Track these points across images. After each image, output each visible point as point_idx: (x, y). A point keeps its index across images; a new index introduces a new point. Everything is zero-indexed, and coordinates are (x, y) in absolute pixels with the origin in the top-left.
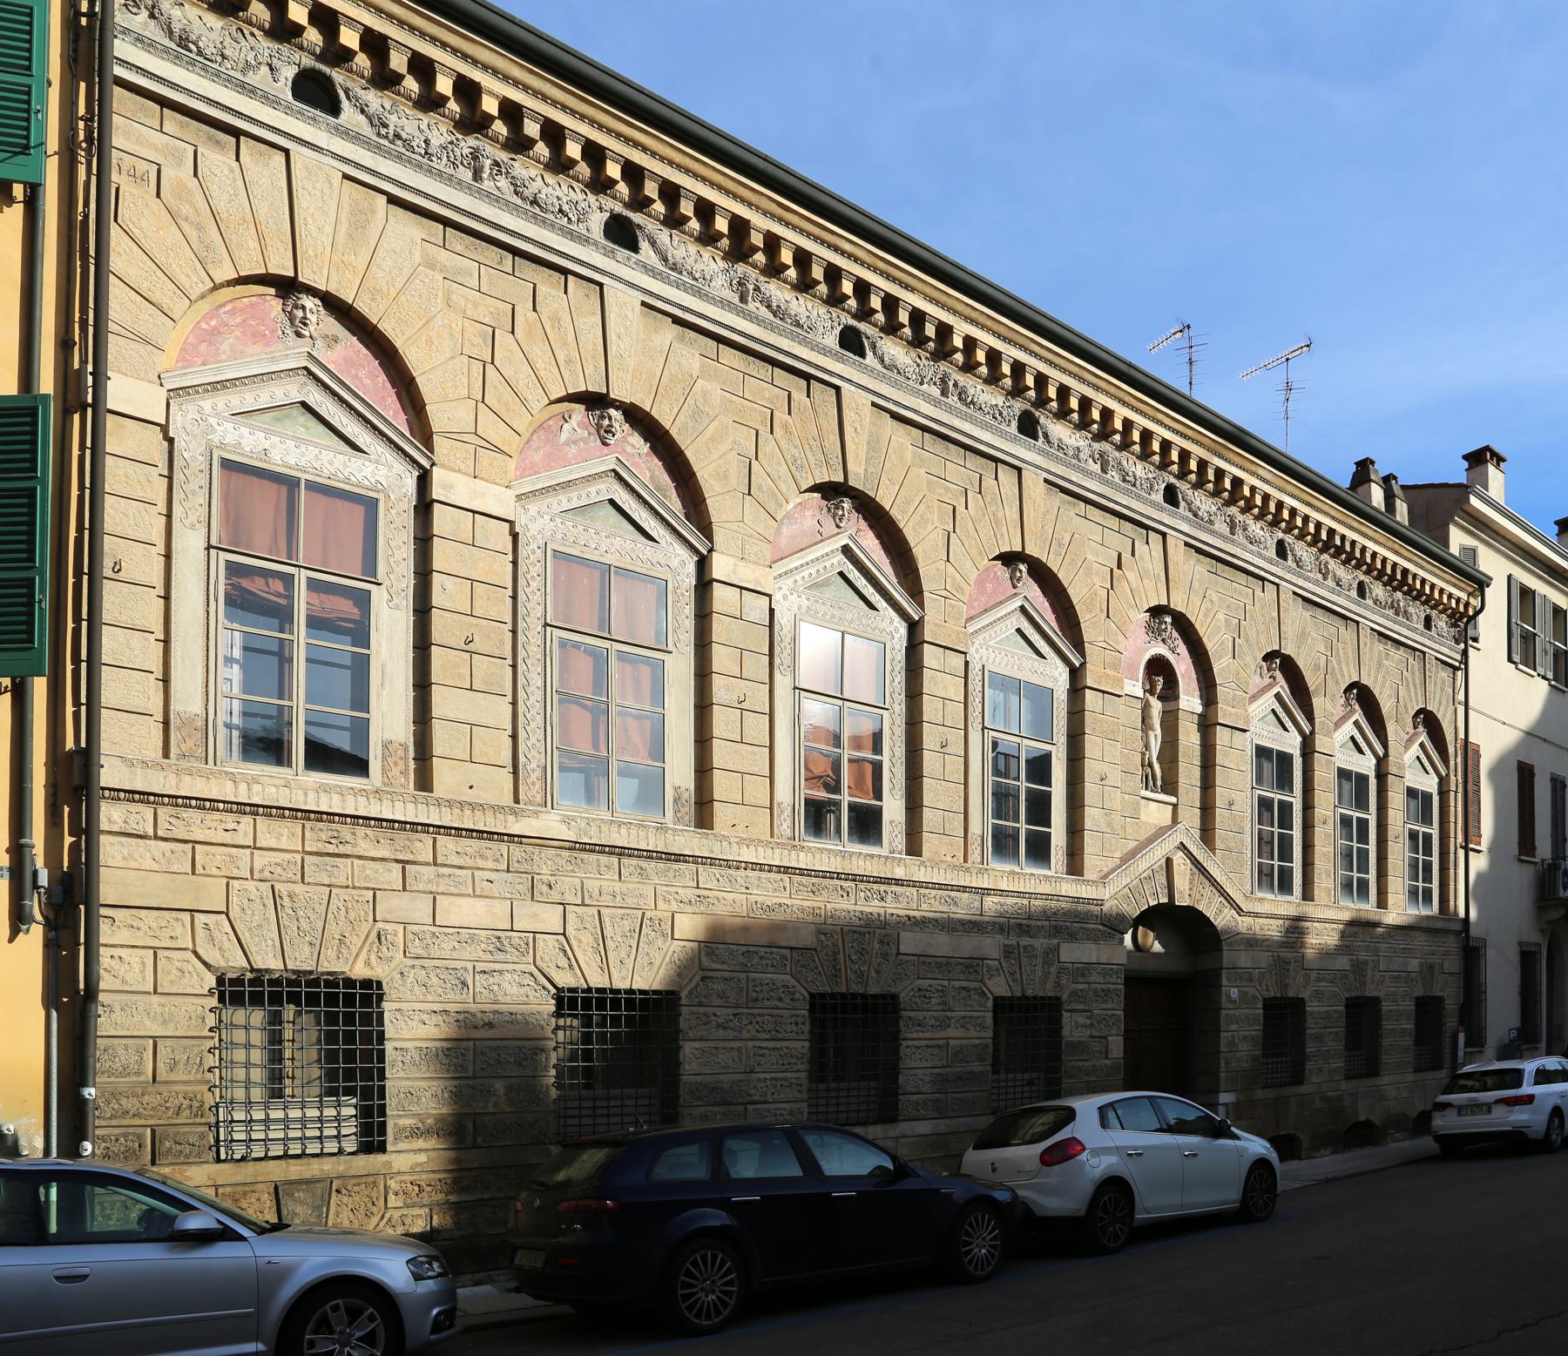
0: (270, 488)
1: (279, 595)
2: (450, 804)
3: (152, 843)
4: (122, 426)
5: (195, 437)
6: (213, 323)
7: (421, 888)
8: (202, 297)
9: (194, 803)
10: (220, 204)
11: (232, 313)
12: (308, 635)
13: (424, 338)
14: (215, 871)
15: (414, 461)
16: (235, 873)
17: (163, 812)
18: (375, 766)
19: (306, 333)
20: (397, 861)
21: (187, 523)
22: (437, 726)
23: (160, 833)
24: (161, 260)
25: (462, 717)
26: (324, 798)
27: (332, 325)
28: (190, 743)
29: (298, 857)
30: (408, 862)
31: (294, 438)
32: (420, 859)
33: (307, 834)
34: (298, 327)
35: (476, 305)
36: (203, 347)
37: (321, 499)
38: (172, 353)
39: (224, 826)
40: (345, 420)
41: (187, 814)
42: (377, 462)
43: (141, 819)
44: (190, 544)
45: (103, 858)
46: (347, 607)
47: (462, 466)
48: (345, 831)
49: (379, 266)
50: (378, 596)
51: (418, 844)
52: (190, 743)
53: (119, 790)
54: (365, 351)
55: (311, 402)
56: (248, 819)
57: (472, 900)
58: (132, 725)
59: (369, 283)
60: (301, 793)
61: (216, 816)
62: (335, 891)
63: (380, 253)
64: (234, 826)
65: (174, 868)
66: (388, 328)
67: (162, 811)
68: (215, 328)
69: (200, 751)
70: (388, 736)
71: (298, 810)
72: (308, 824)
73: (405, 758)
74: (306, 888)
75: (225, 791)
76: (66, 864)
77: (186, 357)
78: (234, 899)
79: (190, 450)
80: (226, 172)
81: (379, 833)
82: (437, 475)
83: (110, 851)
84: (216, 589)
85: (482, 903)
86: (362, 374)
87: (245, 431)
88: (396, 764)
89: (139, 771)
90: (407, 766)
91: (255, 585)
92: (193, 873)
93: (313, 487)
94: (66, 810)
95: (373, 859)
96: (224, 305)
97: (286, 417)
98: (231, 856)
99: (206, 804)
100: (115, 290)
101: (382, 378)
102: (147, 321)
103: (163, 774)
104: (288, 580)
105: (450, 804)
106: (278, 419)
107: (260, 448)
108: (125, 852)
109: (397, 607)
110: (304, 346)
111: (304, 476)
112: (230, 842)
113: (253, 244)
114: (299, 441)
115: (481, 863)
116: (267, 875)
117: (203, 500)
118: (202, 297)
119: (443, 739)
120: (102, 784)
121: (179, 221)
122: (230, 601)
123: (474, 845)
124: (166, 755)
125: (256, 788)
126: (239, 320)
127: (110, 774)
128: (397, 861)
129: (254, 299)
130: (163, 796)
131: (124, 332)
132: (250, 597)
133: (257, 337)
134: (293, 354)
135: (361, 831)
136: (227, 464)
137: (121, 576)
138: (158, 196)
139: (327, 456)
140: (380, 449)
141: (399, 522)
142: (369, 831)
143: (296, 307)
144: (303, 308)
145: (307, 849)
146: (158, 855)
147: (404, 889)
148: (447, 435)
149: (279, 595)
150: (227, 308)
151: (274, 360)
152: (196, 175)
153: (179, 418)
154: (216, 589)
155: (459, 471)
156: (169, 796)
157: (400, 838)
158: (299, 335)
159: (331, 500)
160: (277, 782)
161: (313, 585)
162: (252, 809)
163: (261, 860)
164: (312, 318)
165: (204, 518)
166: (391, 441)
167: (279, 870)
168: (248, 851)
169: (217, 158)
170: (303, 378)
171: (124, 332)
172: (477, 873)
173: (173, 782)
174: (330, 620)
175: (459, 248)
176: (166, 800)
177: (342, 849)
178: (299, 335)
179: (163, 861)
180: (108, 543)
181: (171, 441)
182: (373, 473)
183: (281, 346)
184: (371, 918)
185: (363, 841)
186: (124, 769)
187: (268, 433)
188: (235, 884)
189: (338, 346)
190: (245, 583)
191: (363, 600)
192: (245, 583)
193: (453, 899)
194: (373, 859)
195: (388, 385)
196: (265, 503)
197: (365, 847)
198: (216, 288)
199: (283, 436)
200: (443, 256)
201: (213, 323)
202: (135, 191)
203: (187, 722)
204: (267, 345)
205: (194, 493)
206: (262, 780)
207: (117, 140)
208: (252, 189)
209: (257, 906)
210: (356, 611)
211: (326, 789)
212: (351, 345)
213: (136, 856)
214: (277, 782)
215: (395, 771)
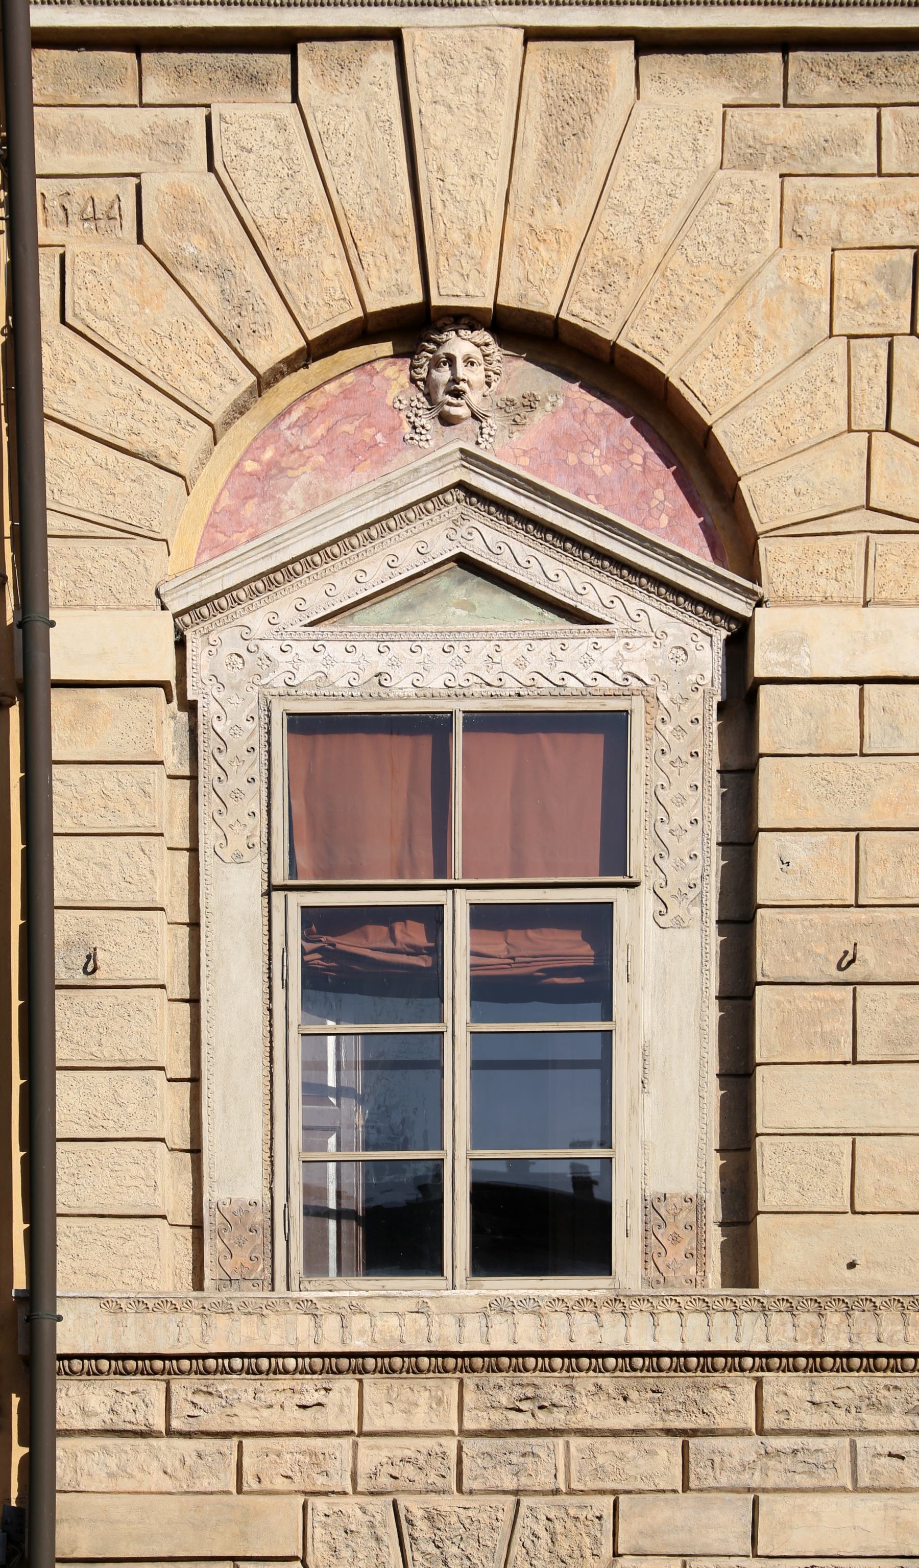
0: (402, 745)
1: (416, 951)
2: (791, 1305)
3: (162, 1443)
4: (93, 706)
5: (236, 688)
6: (268, 454)
7: (724, 1481)
8: (240, 409)
9: (237, 1363)
10: (261, 207)
11: (304, 424)
12: (476, 1017)
13: (733, 329)
14: (280, 1484)
15: (714, 609)
16: (320, 1483)
17: (182, 1387)
18: (625, 1246)
19: (462, 411)
20: (669, 1432)
21: (226, 853)
22: (765, 1148)
23: (176, 1424)
24: (149, 363)
25: (831, 1123)
26: (500, 1323)
27: (524, 375)
28: (242, 1256)
29: (451, 1445)
30: (695, 1433)
31: (438, 635)
32: (722, 1423)
33: (469, 1398)
34: (441, 403)
35: (867, 209)
36: (250, 509)
37: (506, 744)
38: (187, 537)
39: (298, 1399)
40: (552, 567)
41: (223, 1384)
42: (628, 634)
43: (144, 1400)
44: (235, 891)
45: (64, 1473)
46: (569, 946)
47: (832, 589)
48: (552, 1387)
49: (618, 210)
50: (632, 914)
51: (719, 1395)
52: (242, 1256)
53: (97, 1357)
54: (598, 405)
55: (476, 551)
56: (348, 1383)
57: (846, 1500)
58: (126, 1239)
59: (595, 256)
60: (450, 1320)
61: (284, 1382)
62: (526, 1501)
63: (619, 177)
64: (319, 1397)
65: (204, 1484)
66: (640, 340)
67: (179, 1386)
68: (272, 464)
69: (261, 1269)
70: (655, 1187)
71: (445, 1355)
72: (470, 1380)
73: (698, 1226)
74: (464, 1500)
75: (299, 1334)
76: (14, 1494)
77: (216, 537)
78: (317, 1533)
79: (231, 714)
80: (270, 135)
81: (626, 1380)
82: (765, 624)
83: (72, 1461)
84: (285, 966)
85: (875, 1501)
86: (593, 458)
87: (335, 649)
88: (676, 1239)
89: (131, 1318)
90: (701, 1241)
91: (366, 944)
92: (240, 1491)
93: (481, 722)
94: (15, 1400)
95: (615, 1433)
96: (288, 411)
97: (425, 597)
98: (313, 1454)
99: (258, 1363)
100: (59, 452)
101: (641, 451)
102: (139, 494)
103: (177, 1317)
104: (432, 917)
105: (791, 1305)
106: (410, 607)
107: (368, 674)
108: (112, 1462)
109: (679, 923)
110: (461, 438)
111: (458, 707)
112: (309, 1426)
113: (334, 266)
114: (449, 639)
115: (872, 1420)
116: (384, 1481)
117: (256, 804)
118: (240, 409)
119: (777, 1175)
120: (61, 1349)
121: (181, 274)
122: (312, 979)
123: (857, 1384)
124: (198, 1284)
125: (358, 1322)
126: (320, 431)
127: (75, 1330)
128: (669, 1432)
129: (348, 379)
130: (178, 1357)
131: (87, 528)
132: (354, 966)
133: (360, 453)
134: (435, 460)
135: (585, 1381)
136: (300, 724)
137: (101, 977)
138: (140, 240)
139: (511, 651)
140: (633, 606)
141: (680, 747)
142: (604, 1380)
143: (436, 364)
144: (451, 360)
145: (469, 1425)
146: (172, 1463)
147: (686, 1487)
148: (787, 530)
149: (416, 951)
150: (295, 415)
151: (388, 489)
152: (211, 168)
153: (204, 659)
154: (285, 966)
155: (826, 600)
156: (190, 1357)
157: (677, 1386)
158: (446, 420)
159: (528, 739)
160: (401, 1306)
161: (483, 917)
162: (354, 1363)
163: (372, 1454)
164: (475, 375)
165: (258, 838)
166: (657, 581)
167: (409, 1471)
168: (347, 1442)
169: (252, 116)
170: (456, 507)
171: (87, 528)
172: (861, 1442)
173: (196, 1332)
174: (529, 978)
175: (823, 91)
176: (185, 1364)
177: (544, 1420)
178: (446, 420)
179: (182, 1474)
180: (64, 926)
181: (191, 708)
182: (618, 659)
183: (409, 455)
184: (607, 1550)
185: (592, 1401)
186: (105, 1319)
187: (383, 640)
188: (319, 1504)
189: (538, 416)
190: (348, 943)
191: (597, 922)
192: (348, 943)
193: (799, 1499)
194: (615, 1433)
195: (656, 462)
196: (385, 782)
197: (594, 1411)
198: (264, 383)
199: (415, 640)
200: (782, 126)
201: (268, 454)
202: (94, 248)
203: (235, 1220)
204: (382, 461)
205: (237, 795)
206: (368, 1305)
207: (46, 158)
208: (330, 149)
209: (364, 1542)
210: (587, 949)
211: (502, 1307)
212: (568, 403)
213: (132, 1468)
214: (401, 1306)
215: (676, 1253)
